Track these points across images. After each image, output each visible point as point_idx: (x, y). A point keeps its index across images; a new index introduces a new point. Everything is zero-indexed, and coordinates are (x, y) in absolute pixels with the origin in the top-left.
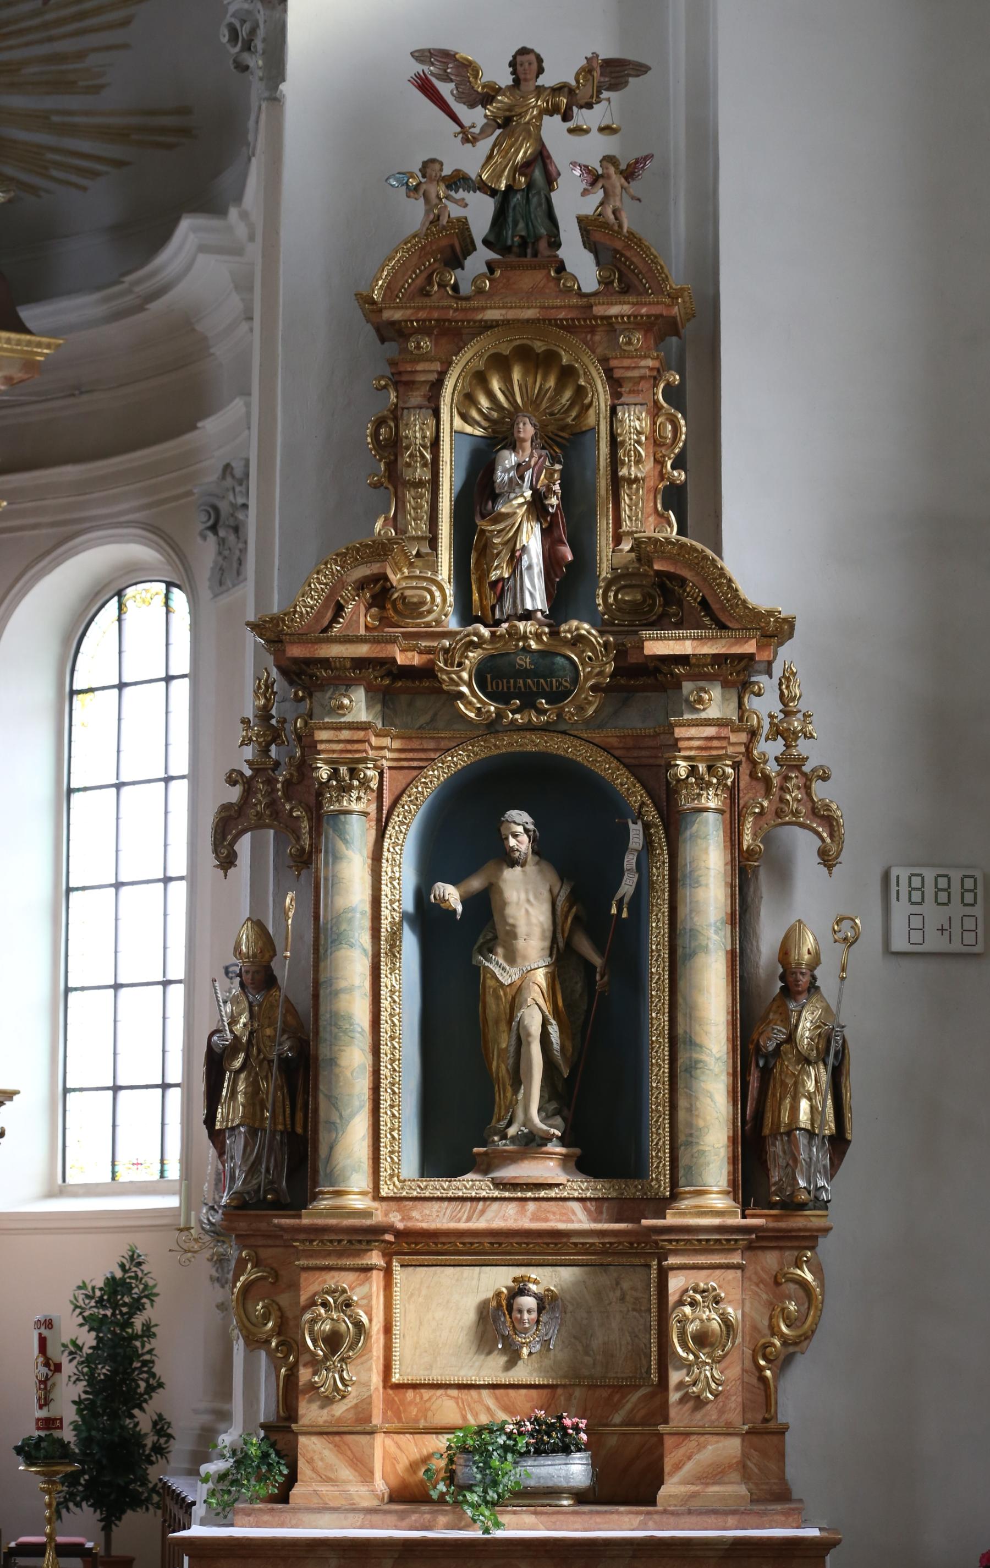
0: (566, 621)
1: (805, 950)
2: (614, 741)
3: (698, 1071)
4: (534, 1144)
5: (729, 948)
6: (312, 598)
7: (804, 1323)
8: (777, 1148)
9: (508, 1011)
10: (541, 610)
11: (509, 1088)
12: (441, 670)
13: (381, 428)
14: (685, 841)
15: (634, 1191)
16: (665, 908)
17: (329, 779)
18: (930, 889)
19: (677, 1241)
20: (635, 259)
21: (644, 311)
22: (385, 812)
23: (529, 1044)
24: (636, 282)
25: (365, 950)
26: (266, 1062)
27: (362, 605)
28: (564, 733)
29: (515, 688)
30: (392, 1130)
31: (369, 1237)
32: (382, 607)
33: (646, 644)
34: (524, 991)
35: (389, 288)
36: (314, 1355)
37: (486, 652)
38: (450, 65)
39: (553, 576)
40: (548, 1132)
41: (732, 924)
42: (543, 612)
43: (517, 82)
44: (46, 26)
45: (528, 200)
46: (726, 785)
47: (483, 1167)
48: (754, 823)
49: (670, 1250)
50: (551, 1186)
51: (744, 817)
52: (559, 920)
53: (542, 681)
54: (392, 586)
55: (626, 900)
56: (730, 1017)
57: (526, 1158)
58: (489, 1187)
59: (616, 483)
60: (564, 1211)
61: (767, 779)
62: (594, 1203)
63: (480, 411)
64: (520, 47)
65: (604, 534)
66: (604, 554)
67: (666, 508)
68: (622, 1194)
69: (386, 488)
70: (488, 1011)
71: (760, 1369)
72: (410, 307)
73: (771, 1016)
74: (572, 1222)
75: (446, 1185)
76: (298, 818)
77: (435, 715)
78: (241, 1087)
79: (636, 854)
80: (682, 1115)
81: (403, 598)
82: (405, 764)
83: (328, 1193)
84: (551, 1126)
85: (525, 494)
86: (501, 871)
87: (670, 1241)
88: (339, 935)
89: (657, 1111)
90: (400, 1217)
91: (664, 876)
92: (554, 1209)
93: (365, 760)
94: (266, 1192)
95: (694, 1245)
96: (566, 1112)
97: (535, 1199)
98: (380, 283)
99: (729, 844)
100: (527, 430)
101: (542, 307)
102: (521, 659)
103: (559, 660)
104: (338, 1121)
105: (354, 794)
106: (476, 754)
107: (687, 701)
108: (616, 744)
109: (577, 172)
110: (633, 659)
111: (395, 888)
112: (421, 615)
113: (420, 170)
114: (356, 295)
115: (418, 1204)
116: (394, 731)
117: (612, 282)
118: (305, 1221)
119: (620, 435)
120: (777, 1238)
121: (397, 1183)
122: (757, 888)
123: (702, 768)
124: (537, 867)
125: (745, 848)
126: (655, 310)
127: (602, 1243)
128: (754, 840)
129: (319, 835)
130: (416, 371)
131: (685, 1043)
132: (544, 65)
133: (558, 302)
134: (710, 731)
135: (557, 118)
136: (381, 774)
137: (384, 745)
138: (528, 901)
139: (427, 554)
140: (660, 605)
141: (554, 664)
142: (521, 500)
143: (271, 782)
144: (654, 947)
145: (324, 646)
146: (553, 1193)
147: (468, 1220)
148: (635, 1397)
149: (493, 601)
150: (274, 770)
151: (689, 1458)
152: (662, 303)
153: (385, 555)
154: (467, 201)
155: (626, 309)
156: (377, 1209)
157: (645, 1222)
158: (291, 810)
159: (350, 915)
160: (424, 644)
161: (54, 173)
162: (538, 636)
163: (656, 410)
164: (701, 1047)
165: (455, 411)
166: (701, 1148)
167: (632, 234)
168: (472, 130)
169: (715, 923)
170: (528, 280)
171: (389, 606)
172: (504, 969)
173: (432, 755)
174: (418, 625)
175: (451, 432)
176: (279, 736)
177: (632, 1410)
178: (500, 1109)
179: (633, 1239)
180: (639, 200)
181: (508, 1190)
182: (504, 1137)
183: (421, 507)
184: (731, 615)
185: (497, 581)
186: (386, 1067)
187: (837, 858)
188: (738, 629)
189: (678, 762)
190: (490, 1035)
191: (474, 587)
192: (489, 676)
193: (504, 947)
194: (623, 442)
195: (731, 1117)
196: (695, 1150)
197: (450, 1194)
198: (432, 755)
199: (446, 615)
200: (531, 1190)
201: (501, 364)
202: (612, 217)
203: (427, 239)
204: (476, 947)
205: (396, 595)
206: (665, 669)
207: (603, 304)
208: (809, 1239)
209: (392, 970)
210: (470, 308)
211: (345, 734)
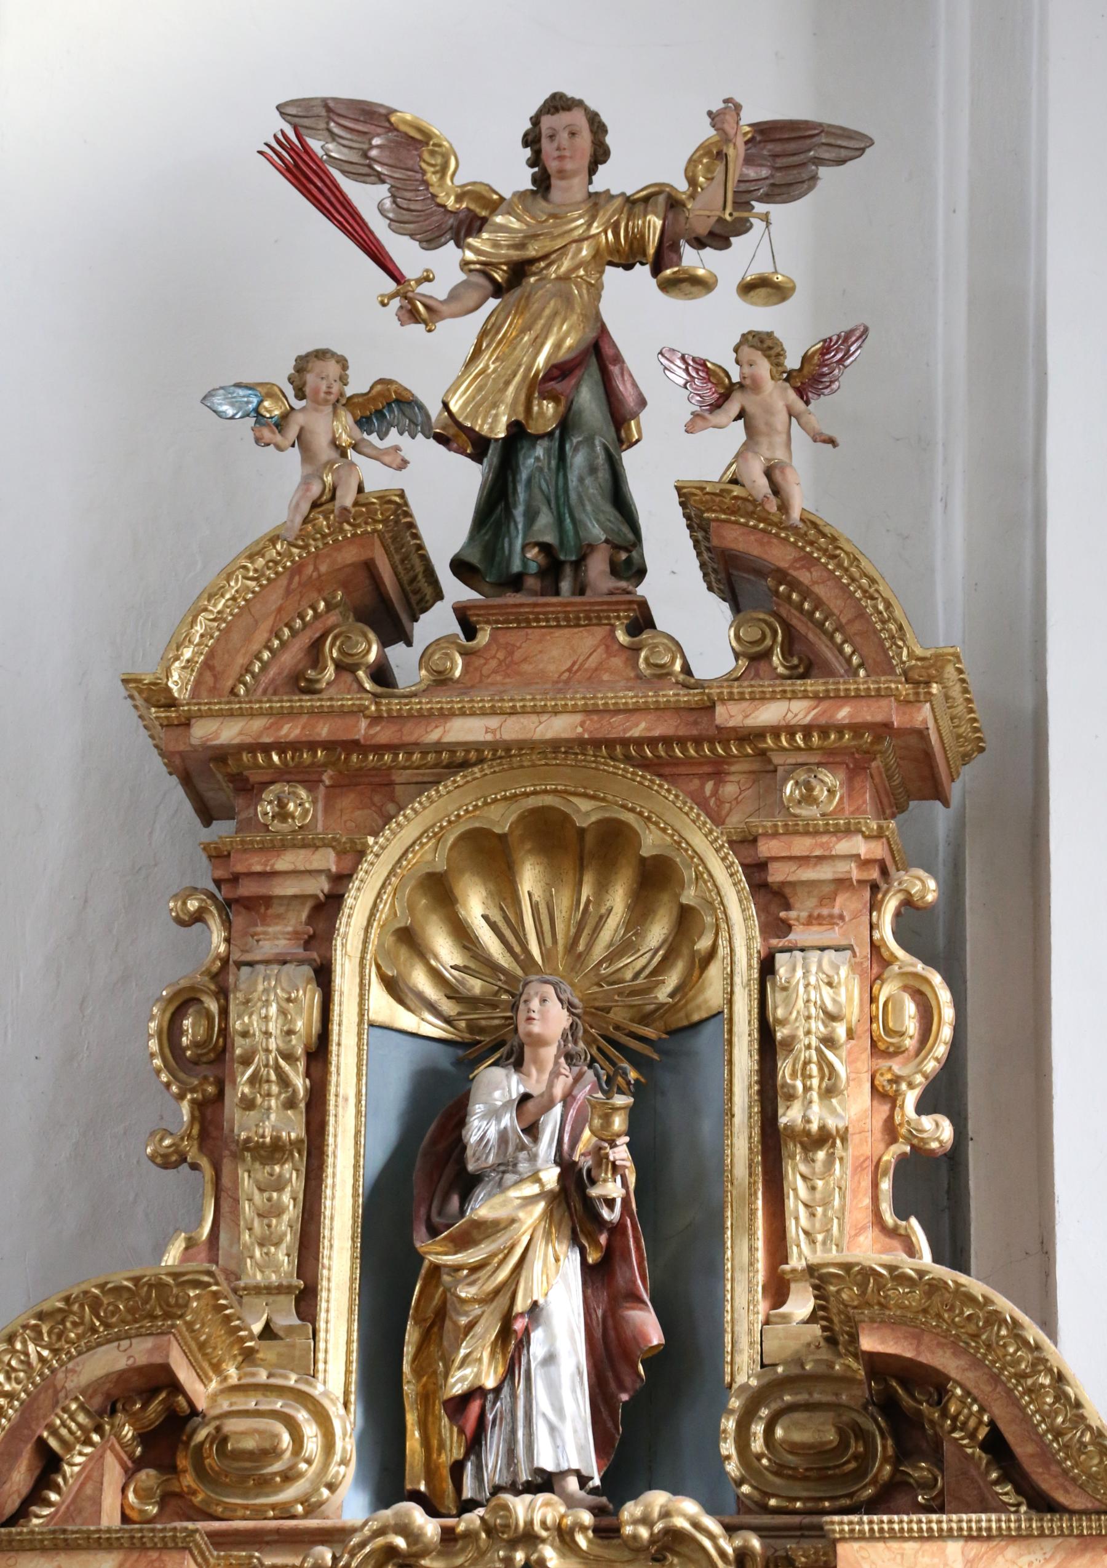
0: (634, 1496)
10: (578, 1473)
13: (184, 1016)
20: (820, 590)
21: (843, 714)
24: (829, 654)
27: (110, 1459)
32: (169, 1469)
33: (841, 1548)
38: (376, 141)
39: (613, 1385)
42: (583, 1480)
43: (543, 183)
45: (562, 457)
54: (194, 1412)
63: (436, 975)
64: (547, 95)
65: (742, 1280)
66: (742, 1328)
67: (901, 1213)
69: (194, 1167)
72: (261, 713)
81: (221, 1439)
85: (543, 1175)
98: (187, 653)
101: (587, 711)
109: (679, 376)
112: (265, 1484)
113: (291, 380)
114: (125, 681)
117: (767, 654)
119: (782, 1023)
126: (872, 712)
130: (274, 874)
132: (609, 140)
133: (629, 698)
135: (642, 272)
139: (290, 1330)
140: (885, 1460)
142: (532, 1189)
152: (889, 694)
153: (167, 1315)
154: (405, 453)
155: (799, 711)
167: (815, 525)
168: (425, 289)
174: (259, 1513)
175: (361, 1022)
180: (832, 442)
183: (278, 1211)
185: (465, 1399)
188: (1086, 1512)
191: (411, 1418)
194: (789, 1044)
199: (332, 1487)
202: (763, 482)
203: (305, 547)
205: (202, 1434)
207: (742, 698)
210: (410, 716)
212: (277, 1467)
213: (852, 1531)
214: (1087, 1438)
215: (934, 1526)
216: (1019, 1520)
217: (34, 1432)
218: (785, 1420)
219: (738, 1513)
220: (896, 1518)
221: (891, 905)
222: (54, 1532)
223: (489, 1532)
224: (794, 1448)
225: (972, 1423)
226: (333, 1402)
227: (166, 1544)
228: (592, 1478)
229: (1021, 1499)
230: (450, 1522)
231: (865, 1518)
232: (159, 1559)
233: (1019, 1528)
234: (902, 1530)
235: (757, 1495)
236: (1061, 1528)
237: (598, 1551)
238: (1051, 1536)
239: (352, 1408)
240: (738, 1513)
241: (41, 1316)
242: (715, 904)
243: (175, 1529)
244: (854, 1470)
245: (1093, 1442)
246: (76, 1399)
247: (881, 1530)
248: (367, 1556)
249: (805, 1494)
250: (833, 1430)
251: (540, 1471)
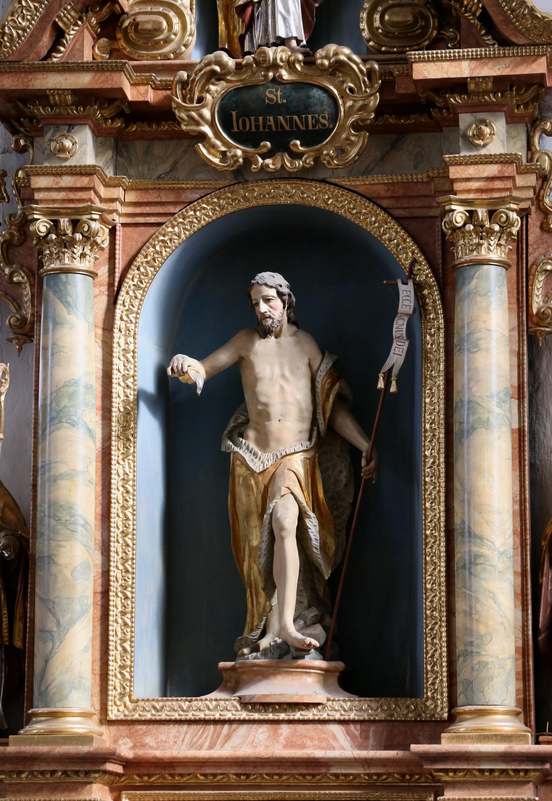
0: (321, 47)
2: (381, 190)
3: (479, 568)
4: (289, 656)
5: (516, 426)
6: (23, 18)
9: (260, 503)
10: (296, 38)
11: (262, 594)
12: (179, 106)
14: (462, 300)
15: (405, 712)
16: (441, 381)
17: (49, 232)
19: (455, 771)
22: (118, 275)
23: (282, 539)
25: (90, 431)
27: (86, 33)
28: (324, 181)
29: (264, 127)
30: (123, 641)
31: (87, 768)
32: (113, 38)
33: (415, 66)
34: (277, 479)
37: (230, 85)
40: (303, 641)
41: (519, 399)
42: (299, 42)
46: (511, 234)
47: (231, 684)
48: (546, 283)
49: (446, 782)
50: (308, 706)
51: (534, 275)
52: (320, 399)
53: (296, 117)
54: (123, 12)
55: (395, 371)
56: (517, 507)
57: (279, 673)
58: (235, 707)
60: (323, 736)
62: (358, 726)
68: (392, 715)
70: (238, 503)
74: (334, 749)
75: (185, 705)
76: (19, 284)
77: (176, 163)
79: (406, 318)
80: (459, 620)
81: (135, 25)
82: (141, 220)
83: (43, 715)
84: (310, 636)
86: (253, 342)
87: (446, 771)
88: (59, 412)
89: (432, 616)
90: (131, 744)
91: (439, 345)
92: (312, 733)
93: (88, 210)
95: (475, 776)
96: (328, 620)
97: (290, 722)
99: (515, 306)
102: (271, 92)
103: (316, 93)
104: (55, 629)
105: (78, 250)
106: (222, 208)
107: (465, 137)
108: (383, 193)
110: (401, 89)
111: (128, 361)
112: (157, 45)
115: (153, 728)
116: (126, 181)
118: (11, 749)
121: (128, 703)
123: (482, 213)
124: (294, 338)
125: (535, 311)
127: (369, 775)
128: (545, 302)
131: (463, 535)
134: (492, 170)
136: (113, 232)
137: (115, 196)
138: (283, 376)
140: (434, 28)
141: (309, 97)
144: (428, 426)
145: (40, 76)
146: (309, 715)
147: (211, 747)
156: (101, 735)
157: (415, 748)
158: (11, 275)
159: (71, 389)
160: (159, 78)
162: (290, 65)
164: (481, 538)
166: (483, 659)
169: (498, 394)
171: (119, 35)
172: (255, 454)
173: (172, 209)
178: (253, 617)
179: (404, 770)
181: (259, 711)
182: (255, 649)
184: (516, 28)
186: (117, 567)
189: (453, 207)
190: (242, 532)
191: (220, 16)
192: (234, 113)
193: (256, 429)
195: (520, 624)
196: (475, 662)
197: (190, 716)
198: (172, 209)
199: (186, 46)
200: (285, 711)
204: (226, 432)
205: (127, 23)
206: (439, 102)
209: (126, 455)
211: (67, 181)
212: (161, 37)
213: (420, 58)
214: (526, 12)
215: (457, 54)
216: (494, 50)
217: (52, 19)
218: (390, 11)
219: (368, 54)
220: (439, 51)
222: (63, 63)
223: (257, 65)
224: (393, 24)
225: (474, 9)
226: (186, 8)
227: (113, 69)
228: (302, 41)
229: (495, 42)
230: (239, 60)
231: (426, 52)
232: (110, 75)
233: (494, 54)
234: (442, 57)
235: (376, 46)
236: (513, 53)
237: (306, 71)
238: (509, 56)
239: (194, 11)
240: (368, 54)
243: (117, 62)
244: (420, 33)
245: (528, 14)
246: (70, 4)
247: (433, 57)
248: (203, 75)
249: (398, 45)
250: (411, 16)
251: (279, 38)
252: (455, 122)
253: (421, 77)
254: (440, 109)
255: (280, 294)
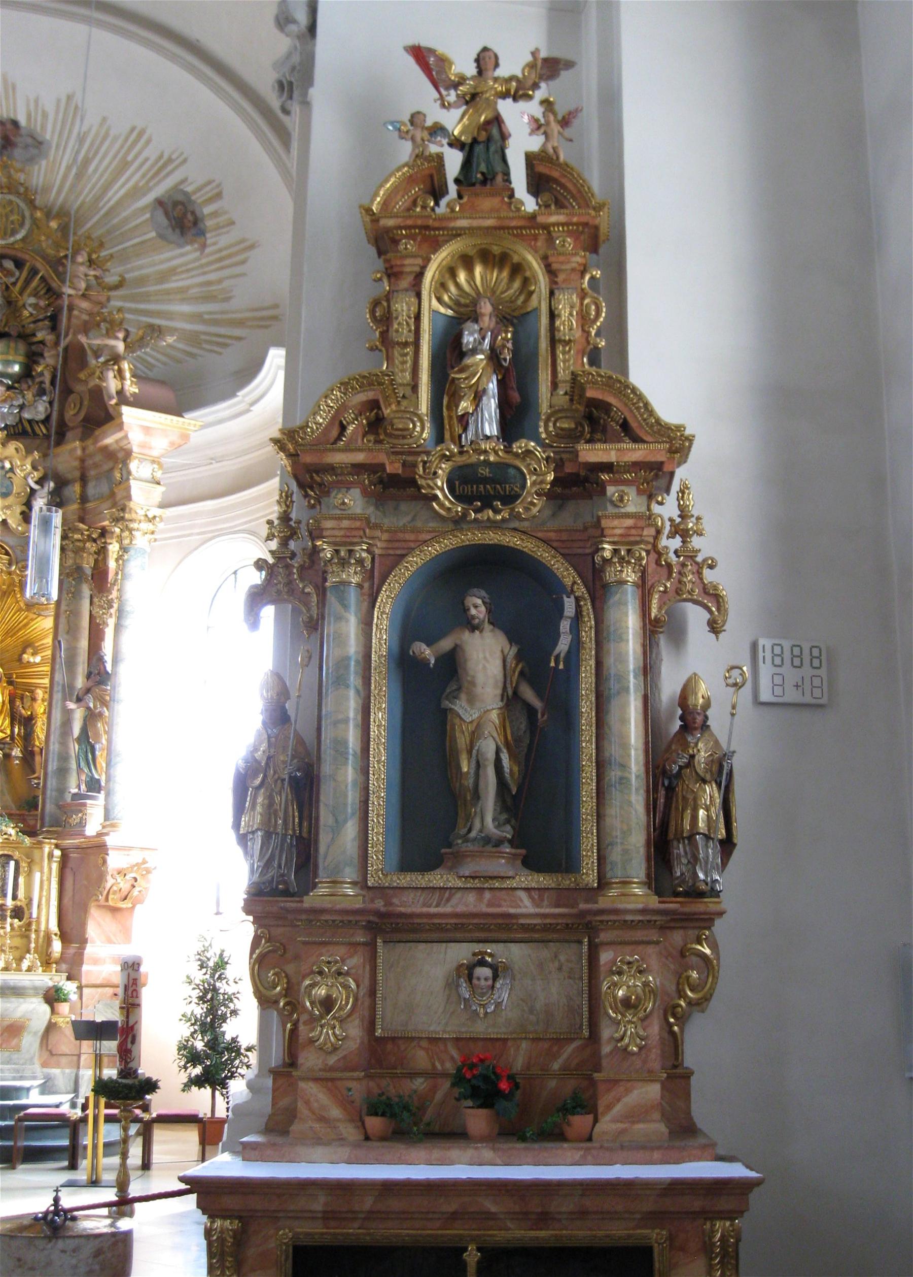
1: (700, 695)
7: (703, 988)
8: (680, 849)
16: (592, 662)
18: (787, 655)
23: (485, 766)
26: (279, 781)
35: (385, 204)
36: (311, 1013)
43: (480, 72)
44: (202, 266)
45: (488, 149)
48: (660, 599)
54: (384, 418)
55: (562, 655)
59: (553, 342)
61: (669, 566)
62: (537, 892)
69: (380, 351)
71: (671, 1025)
73: (673, 747)
74: (520, 907)
76: (309, 594)
77: (415, 516)
78: (260, 800)
84: (503, 832)
90: (382, 903)
94: (278, 883)
100: (486, 308)
101: (499, 218)
103: (512, 471)
107: (612, 502)
110: (569, 469)
120: (682, 920)
122: (658, 654)
129: (324, 605)
131: (610, 764)
134: (629, 522)
143: (288, 567)
147: (437, 906)
148: (570, 1048)
149: (460, 432)
150: (291, 559)
151: (619, 1100)
155: (561, 218)
161: (204, 346)
163: (583, 295)
165: (433, 296)
170: (487, 203)
172: (466, 710)
176: (295, 533)
177: (568, 1058)
180: (571, 140)
182: (466, 840)
187: (723, 626)
192: (457, 483)
194: (559, 316)
201: (467, 262)
208: (706, 921)
221: (587, 277)
224: (562, 429)
241: (341, 384)
242: (535, 277)
252: (603, 492)
253: (584, 461)
254: (592, 484)
255: (484, 602)
